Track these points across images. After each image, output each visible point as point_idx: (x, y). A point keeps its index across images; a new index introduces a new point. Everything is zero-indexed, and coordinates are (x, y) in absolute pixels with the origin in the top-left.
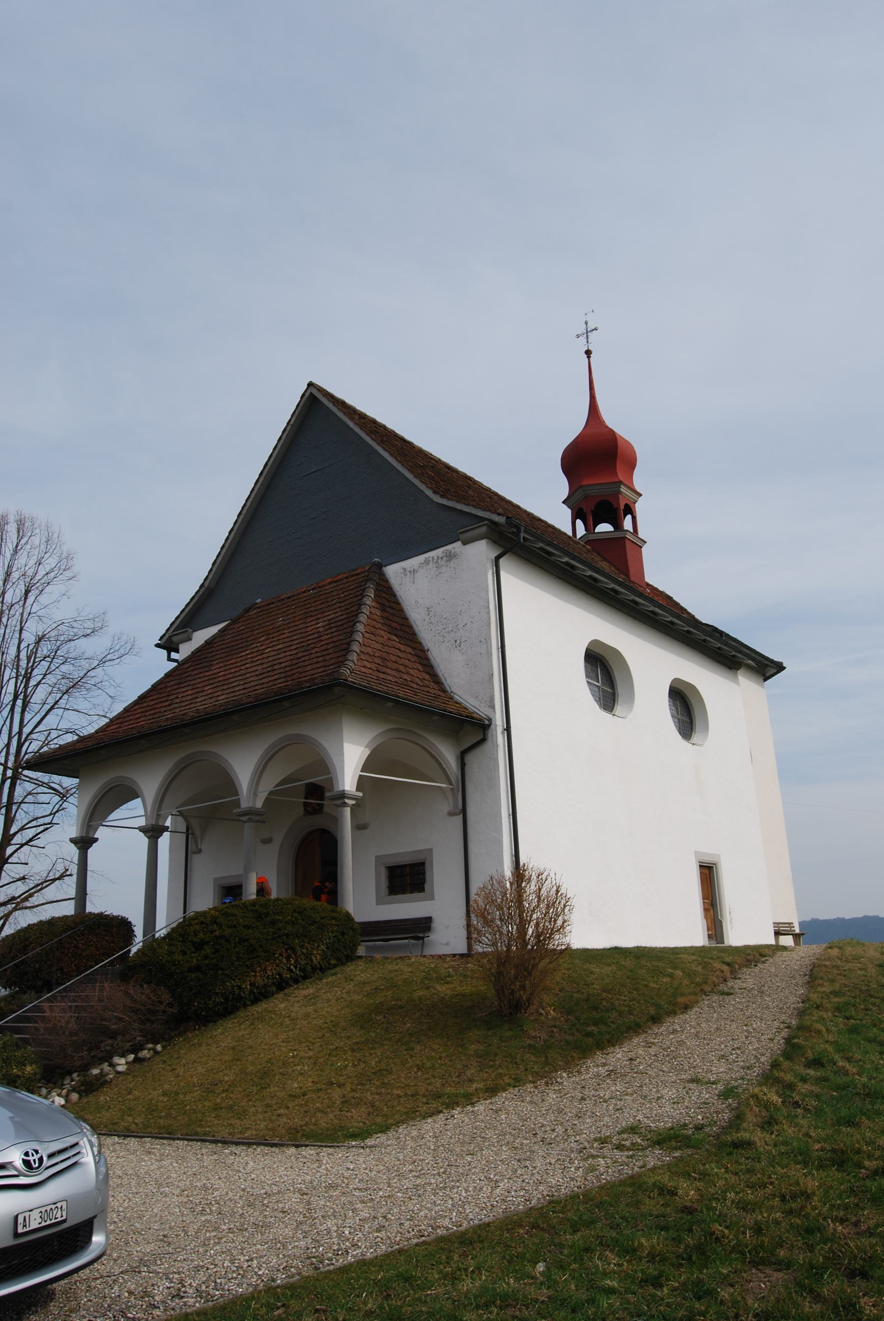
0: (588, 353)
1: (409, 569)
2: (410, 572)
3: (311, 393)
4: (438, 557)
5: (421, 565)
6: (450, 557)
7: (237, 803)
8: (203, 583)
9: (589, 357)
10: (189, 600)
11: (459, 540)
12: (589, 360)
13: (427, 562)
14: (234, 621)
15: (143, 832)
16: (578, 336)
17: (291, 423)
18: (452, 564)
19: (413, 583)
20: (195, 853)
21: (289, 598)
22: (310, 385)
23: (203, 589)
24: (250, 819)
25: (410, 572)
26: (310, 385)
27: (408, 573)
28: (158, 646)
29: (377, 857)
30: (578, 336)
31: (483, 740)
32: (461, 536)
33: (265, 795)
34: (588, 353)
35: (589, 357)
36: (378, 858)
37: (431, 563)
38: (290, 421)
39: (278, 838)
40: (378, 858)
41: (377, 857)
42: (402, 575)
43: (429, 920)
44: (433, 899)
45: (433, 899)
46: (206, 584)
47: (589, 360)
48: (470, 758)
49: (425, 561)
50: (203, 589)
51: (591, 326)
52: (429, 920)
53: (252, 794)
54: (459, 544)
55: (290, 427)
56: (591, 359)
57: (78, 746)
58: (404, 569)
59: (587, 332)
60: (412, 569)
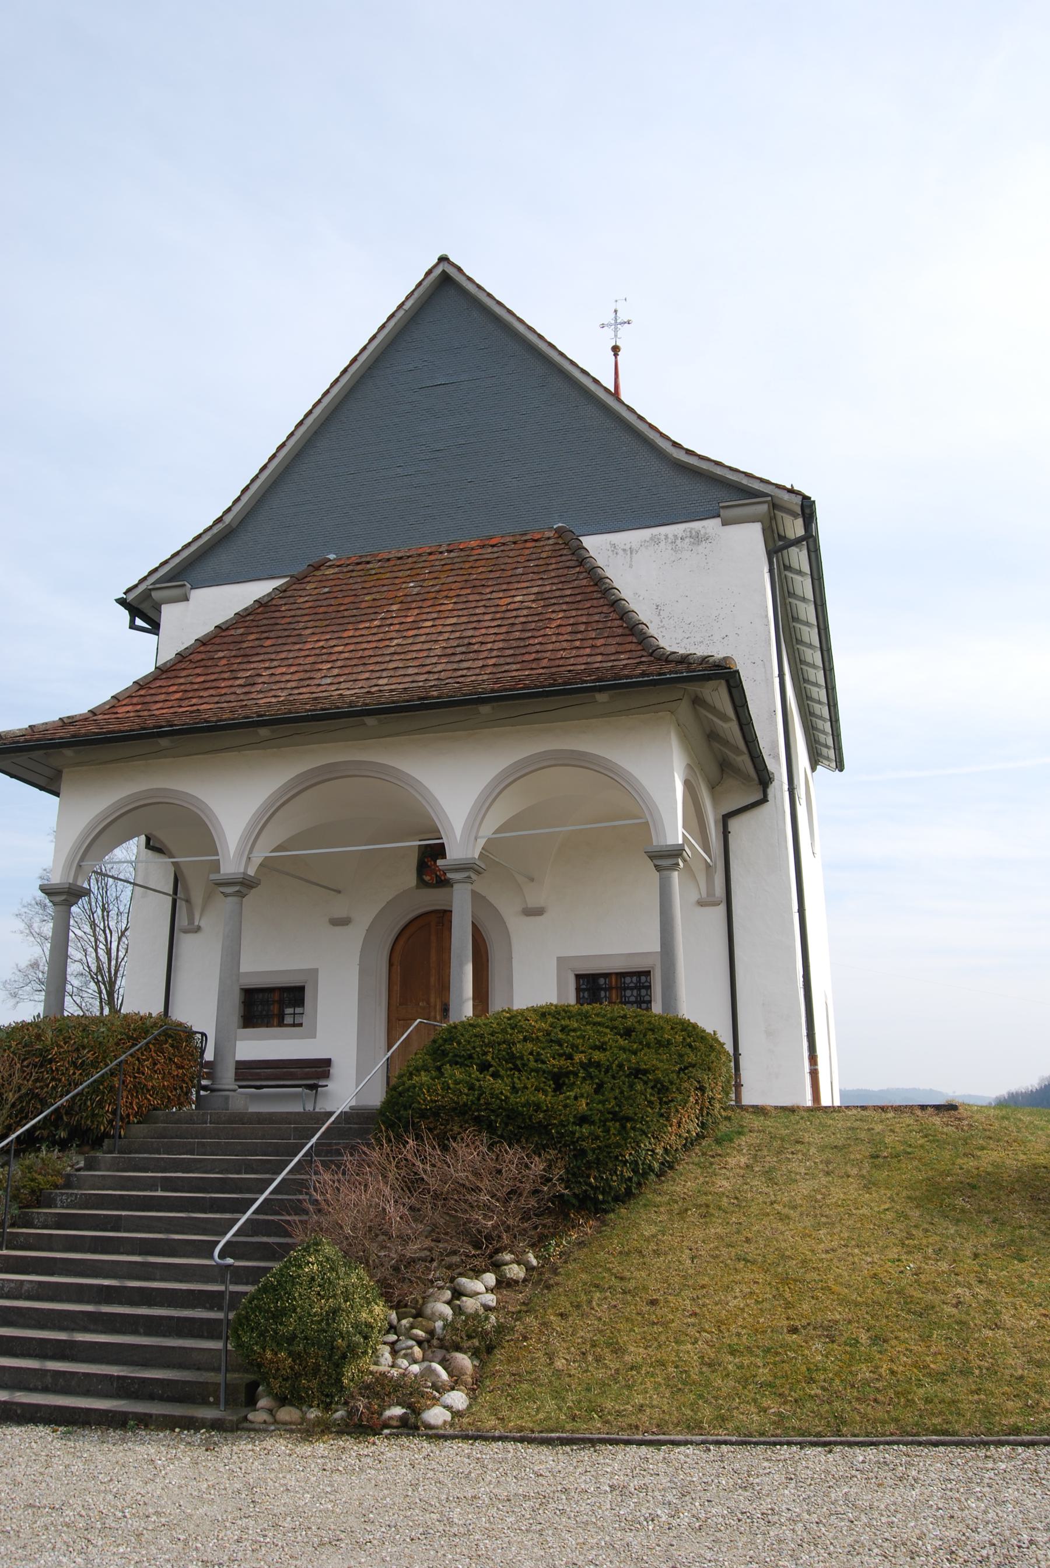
0: (616, 349)
1: (623, 547)
2: (624, 550)
3: (444, 271)
4: (676, 536)
5: (644, 544)
6: (698, 539)
7: (216, 866)
8: (221, 517)
9: (616, 355)
10: (190, 540)
11: (719, 516)
12: (616, 358)
13: (655, 540)
14: (298, 580)
15: (46, 894)
16: (603, 326)
17: (407, 306)
18: (701, 548)
19: (631, 566)
20: (186, 932)
21: (400, 558)
22: (443, 259)
23: (220, 526)
24: (469, 877)
25: (624, 550)
26: (443, 259)
27: (621, 552)
28: (122, 602)
29: (559, 959)
30: (603, 326)
31: (764, 800)
32: (722, 512)
33: (259, 861)
34: (616, 349)
35: (616, 355)
36: (561, 960)
37: (663, 543)
38: (403, 304)
39: (364, 918)
40: (561, 960)
41: (559, 959)
42: (610, 553)
43: (327, 1062)
44: (314, 1036)
45: (314, 1036)
46: (228, 519)
47: (616, 358)
48: (734, 824)
49: (651, 539)
50: (220, 526)
51: (622, 317)
52: (327, 1062)
53: (75, 865)
54: (718, 521)
55: (401, 313)
56: (619, 357)
57: (61, 733)
58: (614, 546)
59: (616, 323)
60: (627, 547)
